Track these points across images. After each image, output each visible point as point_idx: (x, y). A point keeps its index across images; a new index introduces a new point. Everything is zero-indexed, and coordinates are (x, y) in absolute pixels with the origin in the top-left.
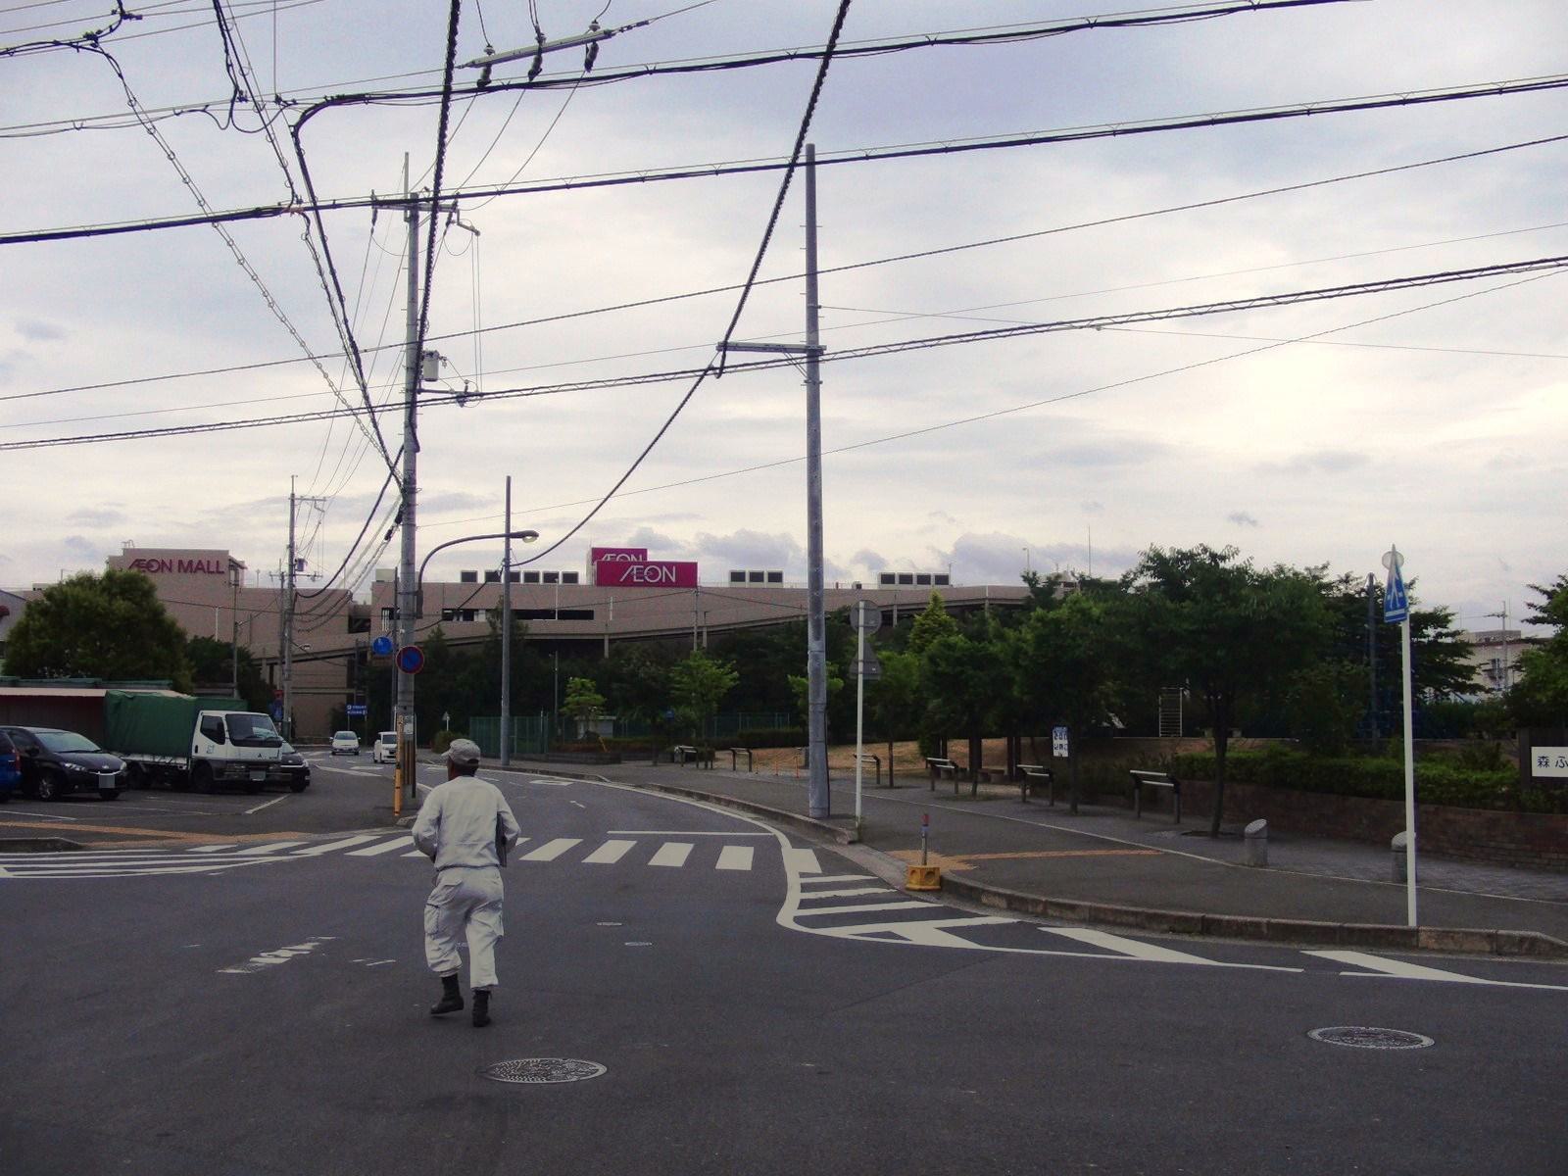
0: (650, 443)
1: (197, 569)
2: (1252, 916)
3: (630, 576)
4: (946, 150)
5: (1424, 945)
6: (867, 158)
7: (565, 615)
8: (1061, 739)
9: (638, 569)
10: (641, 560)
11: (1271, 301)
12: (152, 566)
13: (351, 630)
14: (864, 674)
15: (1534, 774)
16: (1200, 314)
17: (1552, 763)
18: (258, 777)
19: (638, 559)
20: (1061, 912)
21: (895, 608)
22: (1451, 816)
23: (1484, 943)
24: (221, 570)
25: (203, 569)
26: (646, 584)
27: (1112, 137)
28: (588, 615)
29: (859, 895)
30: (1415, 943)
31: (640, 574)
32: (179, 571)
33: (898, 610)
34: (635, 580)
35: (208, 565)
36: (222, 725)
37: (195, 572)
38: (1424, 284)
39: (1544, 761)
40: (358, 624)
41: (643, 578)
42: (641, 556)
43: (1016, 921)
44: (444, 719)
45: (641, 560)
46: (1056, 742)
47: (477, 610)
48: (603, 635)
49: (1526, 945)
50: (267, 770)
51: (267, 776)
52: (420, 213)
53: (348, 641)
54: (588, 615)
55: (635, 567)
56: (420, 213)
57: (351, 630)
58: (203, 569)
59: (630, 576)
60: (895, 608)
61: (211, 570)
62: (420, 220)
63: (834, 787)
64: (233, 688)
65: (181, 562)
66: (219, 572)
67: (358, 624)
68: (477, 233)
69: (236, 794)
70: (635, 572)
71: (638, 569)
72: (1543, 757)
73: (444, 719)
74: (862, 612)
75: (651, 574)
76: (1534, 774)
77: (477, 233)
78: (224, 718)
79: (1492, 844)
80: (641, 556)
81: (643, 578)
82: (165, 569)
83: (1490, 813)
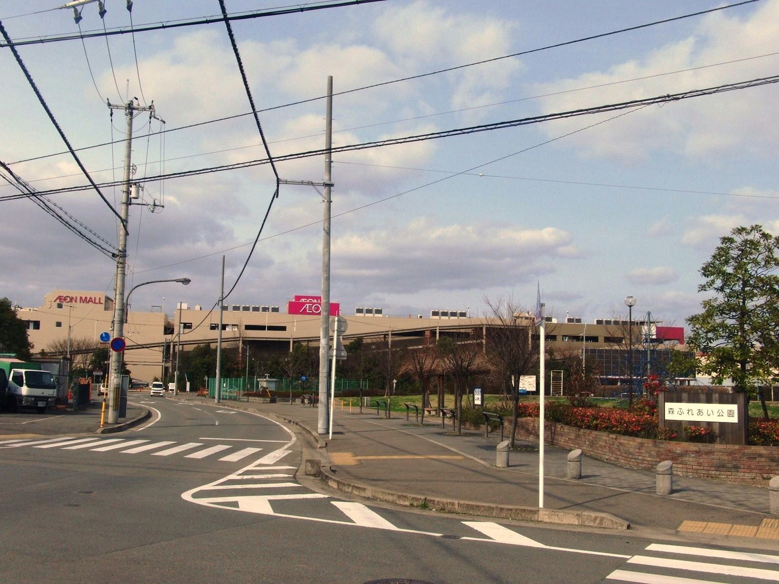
0: (258, 235)
1: (89, 301)
2: (470, 500)
3: (305, 309)
4: (207, 22)
5: (541, 520)
6: (164, 27)
7: (271, 328)
8: (478, 395)
9: (309, 306)
10: (319, 302)
11: (460, 132)
12: (67, 299)
13: (165, 333)
14: (336, 356)
15: (666, 418)
16: (422, 140)
17: (676, 412)
18: (41, 404)
19: (318, 301)
20: (359, 492)
21: (438, 328)
22: (622, 441)
23: (575, 519)
24: (101, 302)
25: (92, 301)
26: (313, 314)
27: (301, 12)
28: (283, 328)
29: (268, 478)
30: (536, 518)
31: (310, 307)
32: (80, 302)
33: (439, 329)
34: (308, 311)
35: (95, 300)
36: (22, 376)
37: (88, 302)
38: (542, 121)
39: (671, 411)
40: (170, 330)
41: (312, 310)
42: (319, 300)
43: (326, 496)
44: (205, 379)
45: (319, 302)
46: (476, 397)
47: (228, 325)
48: (290, 338)
49: (598, 521)
50: (47, 401)
51: (47, 404)
52: (134, 111)
53: (162, 338)
54: (283, 328)
55: (308, 305)
56: (134, 111)
57: (165, 333)
58: (92, 301)
59: (305, 309)
60: (438, 328)
61: (96, 302)
62: (134, 114)
63: (424, 419)
64: (60, 359)
65: (81, 298)
66: (100, 303)
67: (170, 330)
68: (164, 122)
69: (32, 413)
70: (308, 307)
71: (309, 306)
72: (671, 409)
73: (205, 379)
74: (336, 323)
75: (316, 308)
76: (666, 418)
77: (164, 122)
78: (24, 373)
79: (640, 457)
80: (319, 300)
81: (312, 310)
82: (73, 301)
83: (639, 440)
